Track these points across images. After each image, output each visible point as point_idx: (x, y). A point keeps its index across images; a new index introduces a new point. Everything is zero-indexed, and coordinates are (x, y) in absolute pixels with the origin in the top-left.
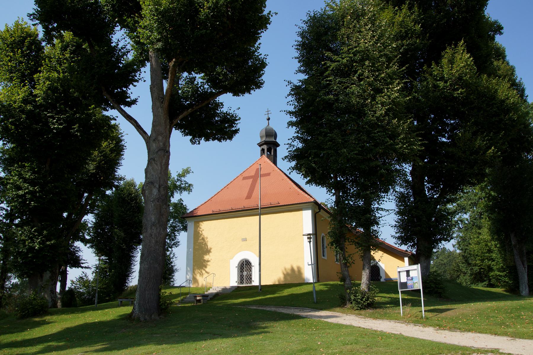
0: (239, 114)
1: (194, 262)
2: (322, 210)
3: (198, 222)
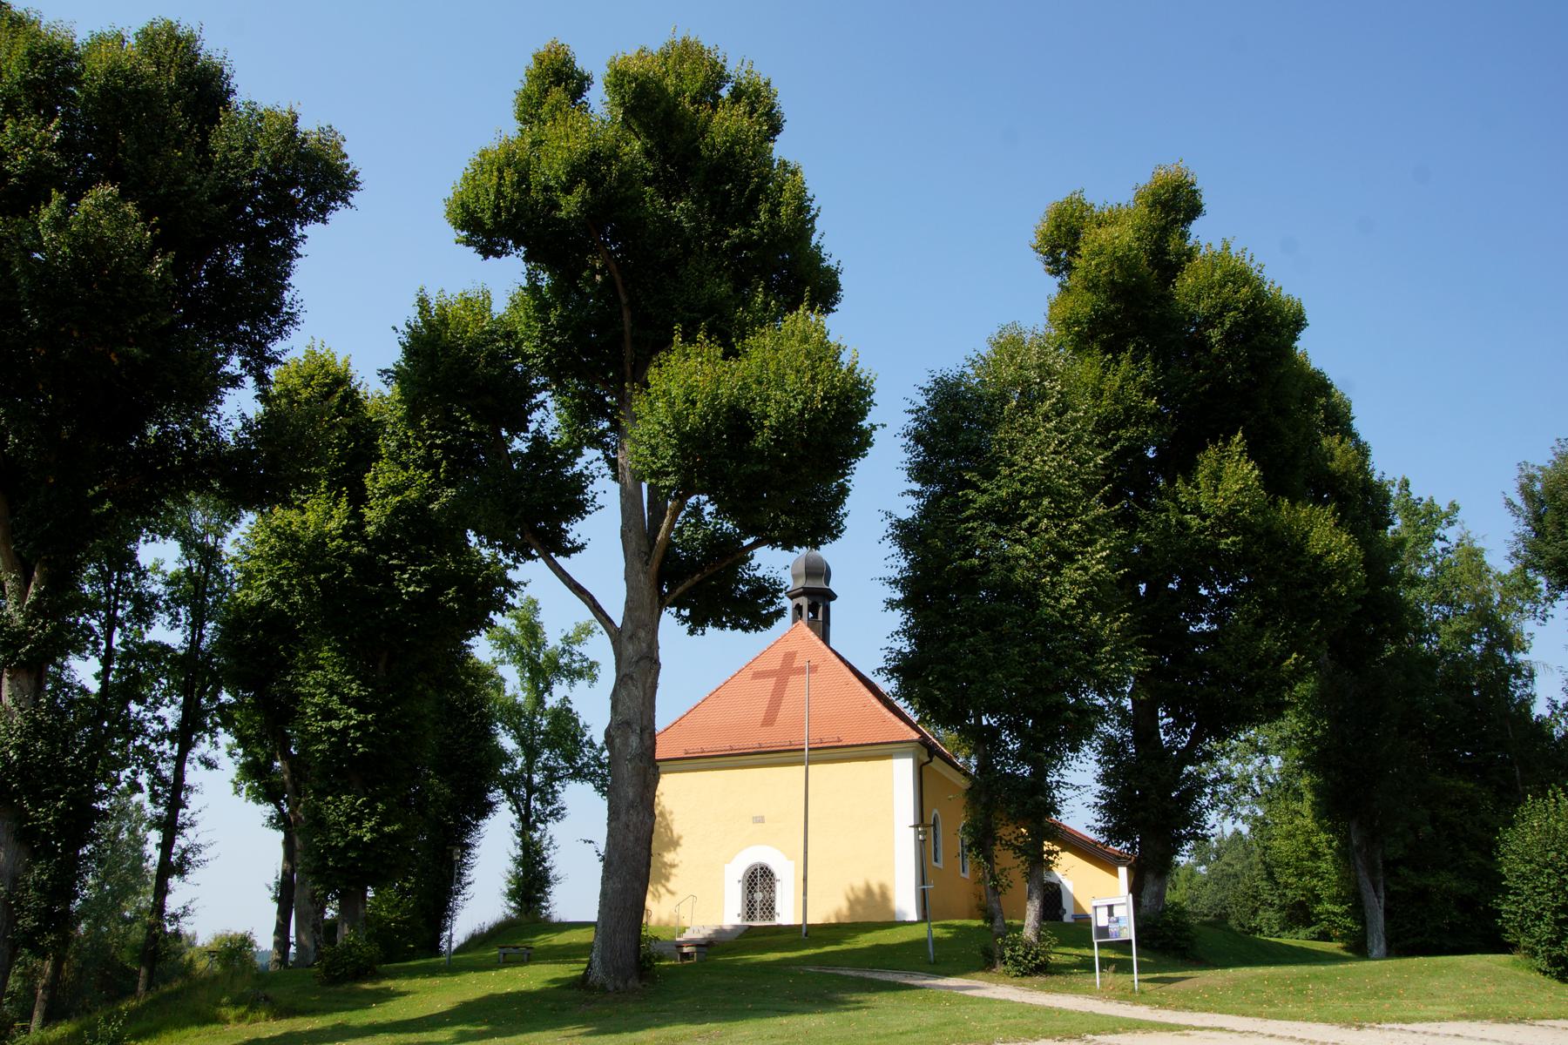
2: (935, 758)
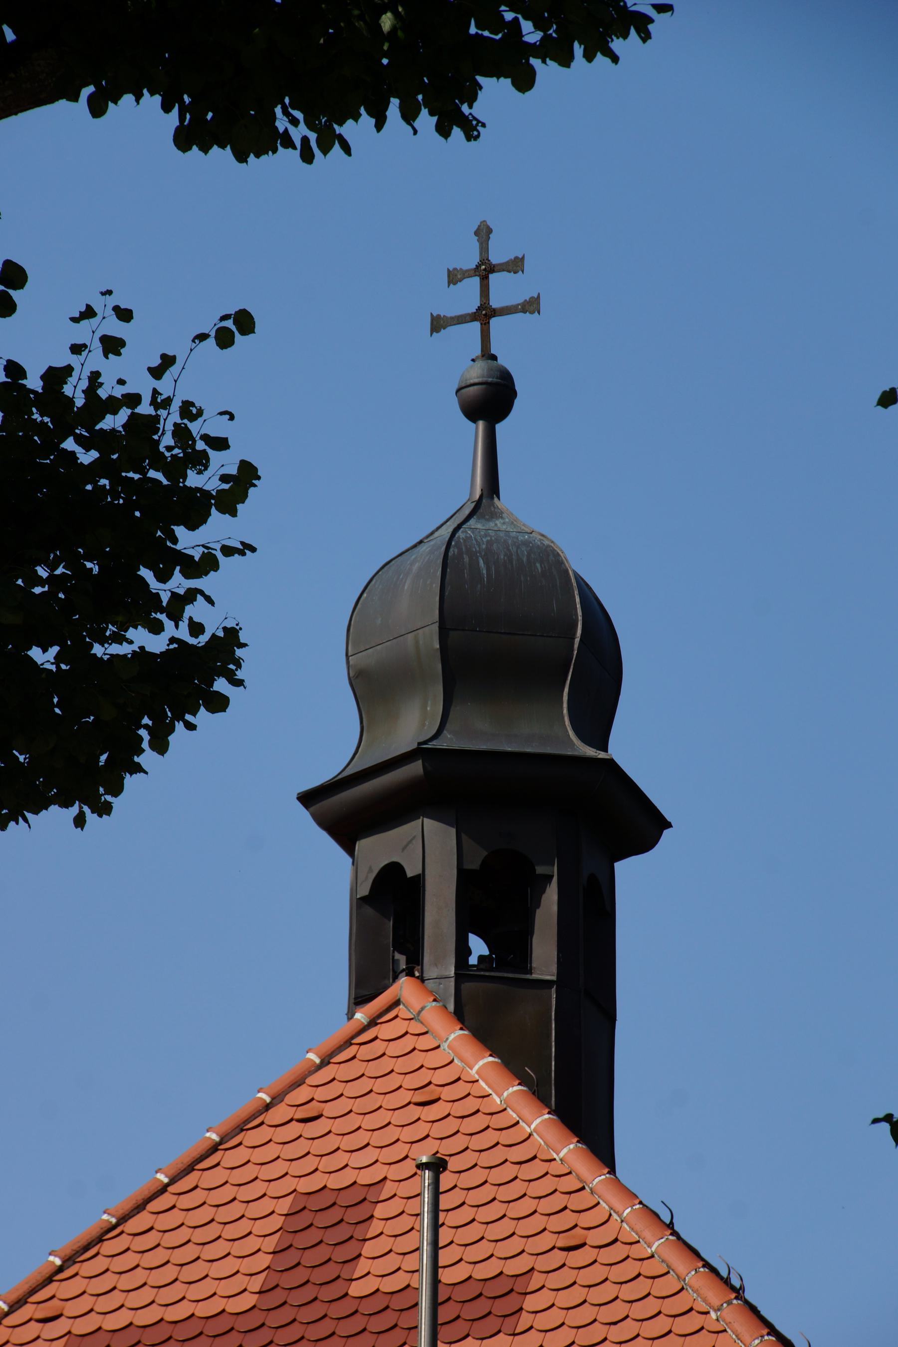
0: (236, 402)
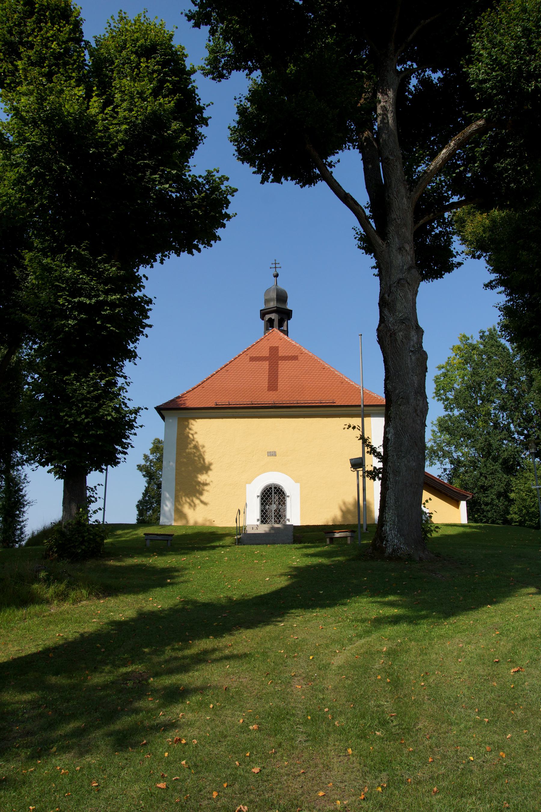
1: (177, 484)
3: (187, 419)
